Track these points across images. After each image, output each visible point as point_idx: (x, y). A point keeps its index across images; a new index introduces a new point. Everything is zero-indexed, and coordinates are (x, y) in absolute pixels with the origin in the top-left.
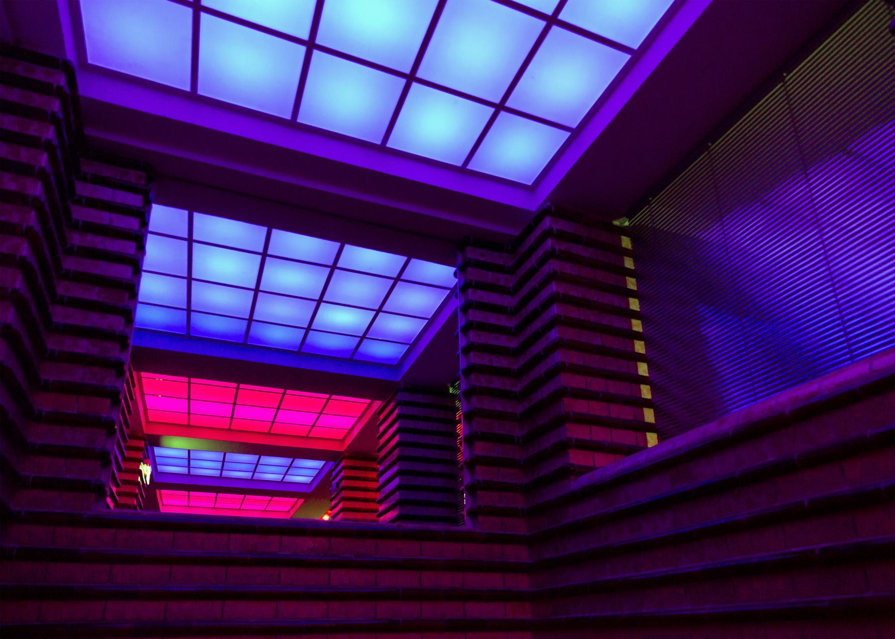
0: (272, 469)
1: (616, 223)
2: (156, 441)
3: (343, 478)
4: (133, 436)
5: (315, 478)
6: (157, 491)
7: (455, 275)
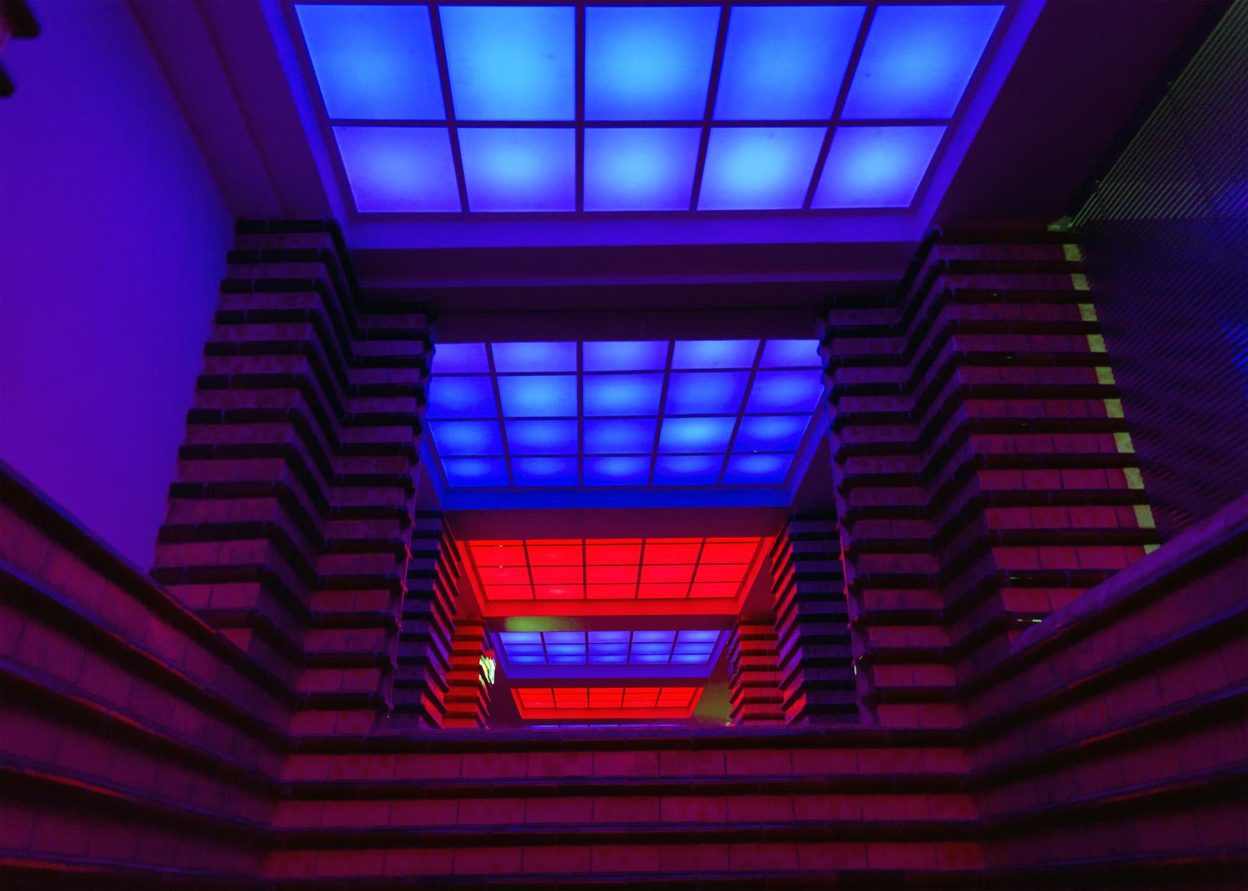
0: (651, 645)
1: (1055, 227)
2: (498, 626)
3: (741, 654)
4: (469, 622)
5: (712, 654)
6: (513, 691)
7: (819, 351)
